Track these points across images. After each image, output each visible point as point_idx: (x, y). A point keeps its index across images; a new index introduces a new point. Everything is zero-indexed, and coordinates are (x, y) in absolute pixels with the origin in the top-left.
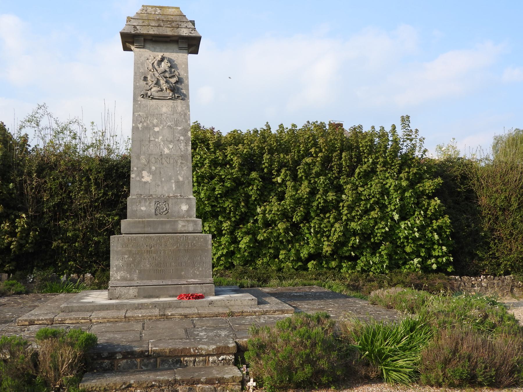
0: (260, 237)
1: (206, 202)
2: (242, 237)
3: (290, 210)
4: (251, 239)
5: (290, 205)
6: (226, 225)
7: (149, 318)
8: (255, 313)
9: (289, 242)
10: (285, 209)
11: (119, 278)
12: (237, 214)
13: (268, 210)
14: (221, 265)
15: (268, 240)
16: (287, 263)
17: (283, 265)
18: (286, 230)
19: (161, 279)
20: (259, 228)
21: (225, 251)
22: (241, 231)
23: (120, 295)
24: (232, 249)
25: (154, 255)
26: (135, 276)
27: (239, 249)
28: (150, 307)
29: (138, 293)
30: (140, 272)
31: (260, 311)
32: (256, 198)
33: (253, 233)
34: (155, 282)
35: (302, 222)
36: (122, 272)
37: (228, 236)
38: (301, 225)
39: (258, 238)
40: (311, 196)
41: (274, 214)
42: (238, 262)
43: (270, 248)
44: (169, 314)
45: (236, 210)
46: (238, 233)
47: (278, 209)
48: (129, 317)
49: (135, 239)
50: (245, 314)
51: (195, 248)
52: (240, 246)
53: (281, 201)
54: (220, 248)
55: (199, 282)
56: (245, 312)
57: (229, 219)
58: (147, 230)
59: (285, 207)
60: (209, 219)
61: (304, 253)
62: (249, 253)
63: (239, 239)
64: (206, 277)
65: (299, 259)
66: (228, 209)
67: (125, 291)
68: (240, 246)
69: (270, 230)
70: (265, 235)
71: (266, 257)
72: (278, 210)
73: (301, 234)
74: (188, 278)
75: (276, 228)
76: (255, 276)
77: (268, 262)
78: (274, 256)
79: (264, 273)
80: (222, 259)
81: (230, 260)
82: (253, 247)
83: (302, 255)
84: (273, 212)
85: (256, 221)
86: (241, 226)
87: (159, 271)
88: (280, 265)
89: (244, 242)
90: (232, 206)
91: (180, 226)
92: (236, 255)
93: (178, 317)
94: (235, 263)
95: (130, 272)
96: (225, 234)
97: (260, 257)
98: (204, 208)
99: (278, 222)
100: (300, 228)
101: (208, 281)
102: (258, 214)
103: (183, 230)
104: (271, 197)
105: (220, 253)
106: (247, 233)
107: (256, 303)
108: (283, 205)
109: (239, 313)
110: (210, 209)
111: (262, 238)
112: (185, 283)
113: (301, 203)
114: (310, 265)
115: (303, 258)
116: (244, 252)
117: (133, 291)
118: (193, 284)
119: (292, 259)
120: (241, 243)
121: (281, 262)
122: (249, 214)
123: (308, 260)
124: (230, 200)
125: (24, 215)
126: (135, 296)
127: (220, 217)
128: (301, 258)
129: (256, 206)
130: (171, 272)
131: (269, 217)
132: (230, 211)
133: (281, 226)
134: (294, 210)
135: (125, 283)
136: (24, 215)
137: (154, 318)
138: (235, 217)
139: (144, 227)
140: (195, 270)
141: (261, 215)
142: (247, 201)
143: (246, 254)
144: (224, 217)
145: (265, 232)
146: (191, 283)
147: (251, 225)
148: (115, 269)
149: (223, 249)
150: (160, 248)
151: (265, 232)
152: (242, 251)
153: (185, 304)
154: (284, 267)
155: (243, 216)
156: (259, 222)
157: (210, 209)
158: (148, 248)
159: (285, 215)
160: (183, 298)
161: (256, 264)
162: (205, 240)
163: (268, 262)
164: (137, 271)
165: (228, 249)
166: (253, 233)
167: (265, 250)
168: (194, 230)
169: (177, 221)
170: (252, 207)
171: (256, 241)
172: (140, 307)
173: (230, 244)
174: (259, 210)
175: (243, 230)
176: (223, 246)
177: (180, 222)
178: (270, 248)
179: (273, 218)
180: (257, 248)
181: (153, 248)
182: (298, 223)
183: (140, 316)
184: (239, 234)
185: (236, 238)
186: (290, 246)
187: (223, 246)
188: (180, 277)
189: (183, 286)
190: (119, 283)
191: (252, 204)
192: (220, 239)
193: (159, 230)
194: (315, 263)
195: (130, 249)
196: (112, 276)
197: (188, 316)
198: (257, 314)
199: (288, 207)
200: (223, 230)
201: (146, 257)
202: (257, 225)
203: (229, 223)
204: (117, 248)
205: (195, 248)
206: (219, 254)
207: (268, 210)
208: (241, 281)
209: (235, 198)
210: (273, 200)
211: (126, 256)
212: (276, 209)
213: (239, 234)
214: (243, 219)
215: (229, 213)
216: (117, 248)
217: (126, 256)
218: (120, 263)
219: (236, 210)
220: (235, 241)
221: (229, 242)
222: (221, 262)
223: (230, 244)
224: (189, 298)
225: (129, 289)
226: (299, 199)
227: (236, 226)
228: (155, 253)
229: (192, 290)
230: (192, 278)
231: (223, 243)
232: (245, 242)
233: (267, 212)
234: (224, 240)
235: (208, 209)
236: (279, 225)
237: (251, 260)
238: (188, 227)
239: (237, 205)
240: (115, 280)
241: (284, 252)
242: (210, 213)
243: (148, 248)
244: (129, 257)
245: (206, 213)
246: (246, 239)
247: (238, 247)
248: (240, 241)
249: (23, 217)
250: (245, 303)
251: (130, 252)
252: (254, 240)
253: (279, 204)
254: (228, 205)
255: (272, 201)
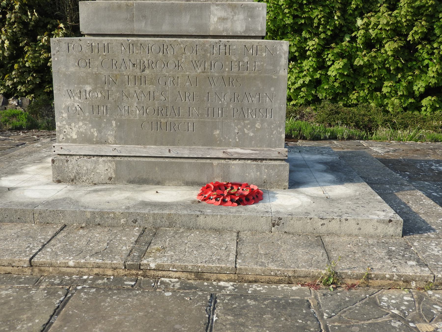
0: (358, 62)
1: (286, 11)
2: (333, 61)
3: (405, 24)
4: (345, 65)
5: (406, 16)
6: (312, 44)
7: (96, 271)
8: (407, 281)
9: (398, 70)
10: (398, 22)
11: (75, 137)
12: (329, 29)
13: (372, 24)
14: (301, 98)
15: (369, 65)
16: (393, 99)
17: (386, 101)
18: (397, 53)
19: (167, 144)
20: (358, 49)
21: (308, 79)
22: (333, 52)
23: (78, 174)
24: (318, 76)
25: (151, 88)
26: (110, 134)
27: (327, 77)
28: (122, 221)
29: (116, 171)
30: (121, 125)
31: (422, 279)
32: (357, 7)
33: (349, 56)
34: (152, 150)
35: (420, 43)
36: (81, 124)
37: (314, 59)
38: (419, 47)
39: (355, 63)
40: (438, 3)
41: (381, 29)
42: (324, 94)
43: (371, 77)
44: (153, 266)
45: (327, 23)
46: (328, 54)
47: (388, 22)
48: (42, 265)
49: (106, 48)
50: (378, 282)
51: (246, 73)
52: (329, 73)
53: (393, 10)
54: (301, 75)
55: (253, 157)
56: (377, 277)
57: (317, 35)
58: (140, 26)
59: (399, 19)
60: (289, 35)
61: (419, 86)
62: (340, 83)
63: (329, 63)
64: (270, 145)
65: (411, 94)
66: (316, 21)
67: (89, 166)
68: (329, 73)
69: (373, 54)
70: (366, 59)
71: (364, 90)
72: (387, 24)
73: (416, 60)
74: (229, 145)
75: (382, 51)
76: (351, 118)
77: (367, 96)
78: (375, 88)
79: (364, 115)
80: (302, 89)
81: (313, 92)
82: (347, 75)
83: (415, 88)
84: (380, 27)
85: (354, 39)
86: (333, 45)
87: (162, 123)
88: (382, 101)
89: (336, 68)
90: (323, 17)
91: (214, 19)
92: (322, 85)
93: (177, 274)
94: (320, 96)
95: (98, 126)
96: (310, 56)
97: (355, 90)
98: (282, 19)
99: (384, 42)
100: (417, 50)
101: (274, 155)
102: (358, 29)
103: (221, 29)
104: (379, 5)
105: (300, 82)
106: (341, 56)
107: (400, 230)
108: (396, 17)
109: (358, 277)
110: (292, 21)
111: (362, 63)
112: (221, 155)
113: (422, 14)
114: (425, 102)
115: (417, 93)
116: (333, 82)
117: (104, 168)
118: (240, 159)
119: (401, 93)
120: (332, 68)
121: (384, 96)
122: (345, 29)
123: (423, 96)
124: (320, 8)
125: (62, 25)
126: (110, 179)
127: (304, 33)
128: (414, 92)
129: (355, 18)
130: (191, 129)
131: (373, 33)
132: (319, 24)
133: (389, 47)
134: (411, 26)
135: (87, 149)
136: (62, 25)
137: (110, 272)
138: (324, 32)
139: (131, 20)
140: (245, 126)
141: (362, 32)
142: (344, 11)
143: (336, 84)
144: (310, 33)
145: (365, 55)
146: (235, 156)
147: (347, 44)
148: (65, 115)
149: (305, 76)
150: (164, 72)
151: (365, 55)
152: (332, 79)
153: (209, 220)
154: (387, 104)
155: (337, 31)
156: (358, 41)
157: (292, 21)
158: (138, 71)
159: (397, 31)
160: (209, 198)
161: (349, 98)
162: (273, 56)
163: (367, 96)
164: (114, 123)
165: (312, 77)
166: (349, 56)
167: (364, 80)
168: (247, 29)
169: (208, 6)
170: (351, 18)
171: (352, 65)
172: (98, 220)
173: (315, 70)
174: (359, 22)
175: (336, 51)
176: (305, 73)
177: (213, 8)
178: (371, 77)
179: (379, 36)
180: (354, 75)
181: (147, 72)
182: (416, 43)
183: (71, 263)
184: (330, 56)
185: (324, 61)
186: (399, 76)
187: (305, 73)
188: (210, 142)
189: (215, 162)
190: (75, 149)
191: (351, 15)
192: (302, 63)
193: (165, 29)
194: (433, 99)
195: (95, 70)
196: (60, 132)
197: (206, 276)
198: (414, 284)
199: (404, 20)
200: (307, 51)
201: (132, 91)
202: (354, 45)
203: (317, 40)
204: (67, 67)
205: (246, 73)
206: (299, 83)
207: (372, 24)
208: (332, 128)
209: (327, 6)
210: (382, 9)
211: (88, 88)
212: (385, 22)
213: (329, 56)
214: (337, 36)
215: (318, 27)
216: (67, 67)
217: (88, 88)
218: (76, 102)
219: (327, 23)
220: (322, 66)
221: (314, 68)
222: (302, 94)
223: (315, 70)
224: (224, 202)
225: (96, 163)
226: (419, 8)
227: (326, 45)
228: (152, 83)
229: (237, 173)
230: (237, 145)
231: (306, 68)
232: (338, 67)
233: (370, 27)
234: (307, 64)
235: (289, 21)
236: (386, 46)
237: (343, 93)
238: (233, 21)
239: (330, 16)
240: (67, 141)
241: (390, 84)
242: (291, 27)
243: (138, 71)
244: (94, 90)
245: (284, 26)
246: (340, 64)
247: (326, 74)
248: (329, 66)
249: (61, 28)
250: (369, 229)
251: (96, 77)
252: (350, 65)
253: (390, 15)
254: (317, 15)
255: (379, 11)
